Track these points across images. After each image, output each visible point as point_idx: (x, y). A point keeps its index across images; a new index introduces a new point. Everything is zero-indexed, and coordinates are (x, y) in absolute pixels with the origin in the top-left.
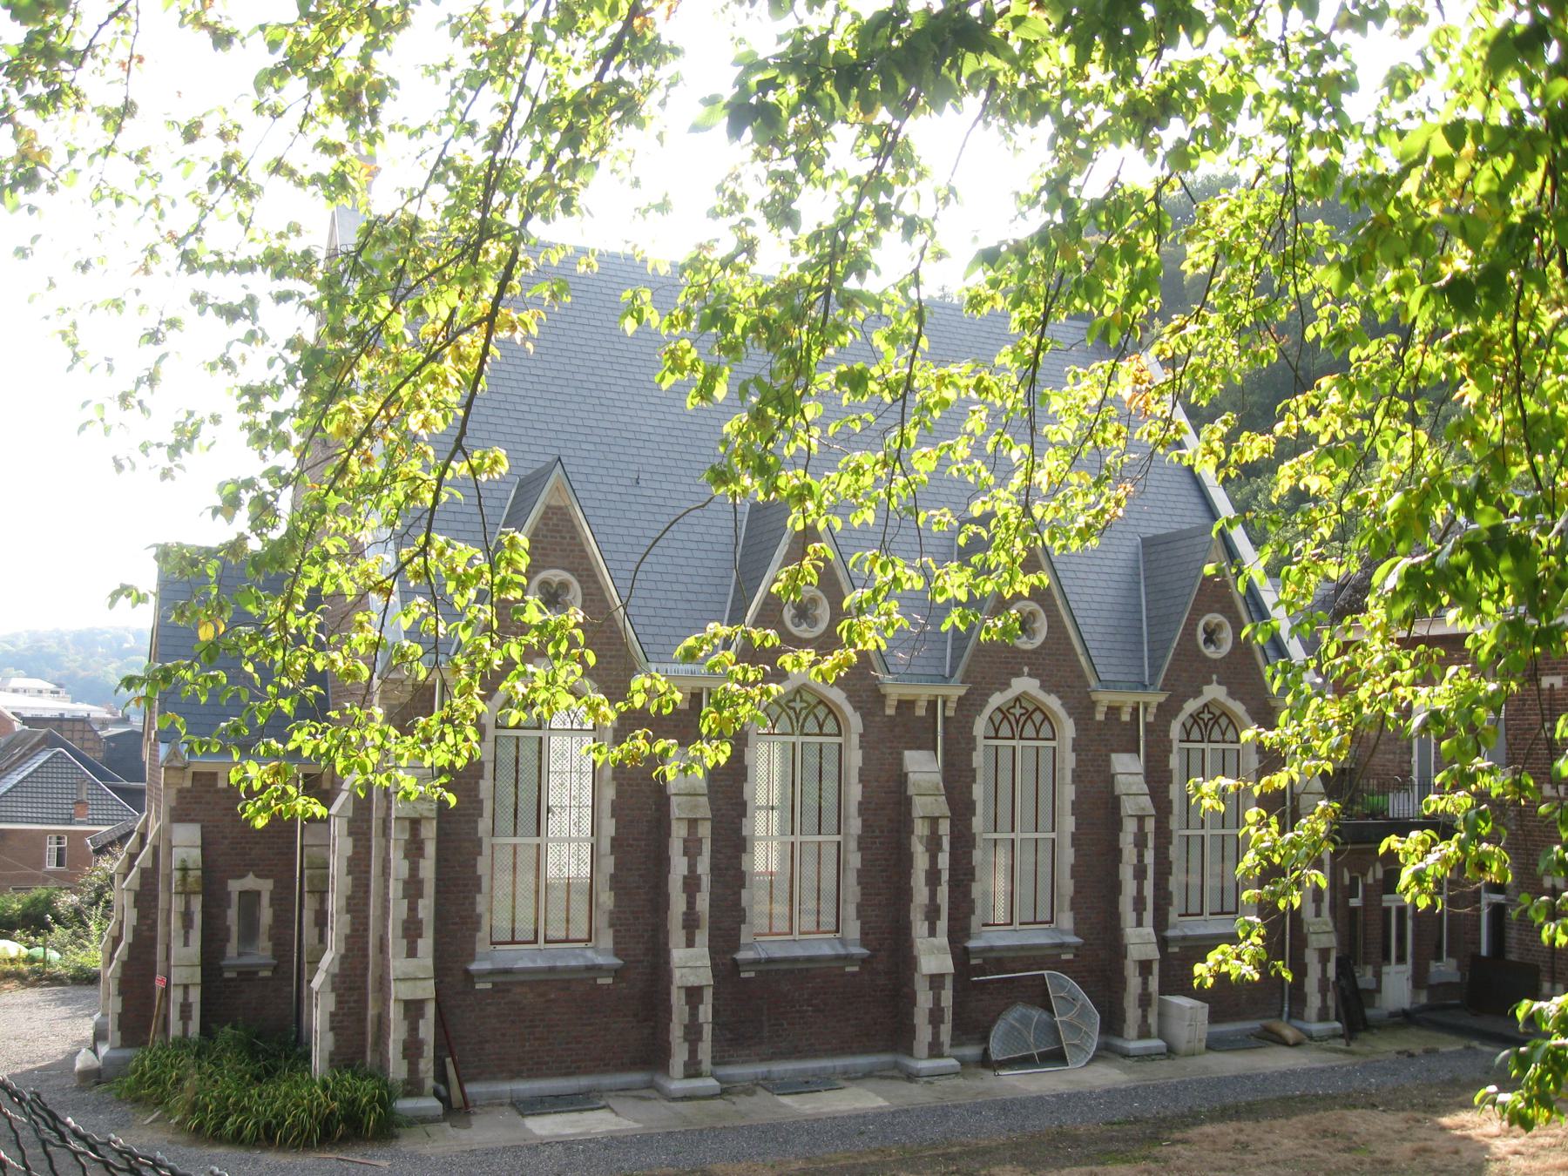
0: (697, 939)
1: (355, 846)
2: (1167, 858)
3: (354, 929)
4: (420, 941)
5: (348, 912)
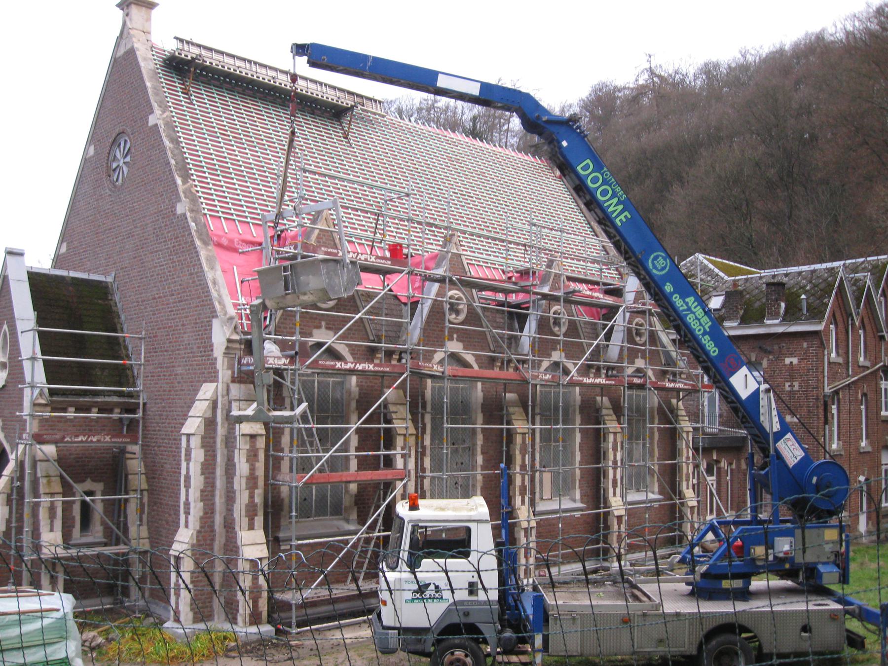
0: (256, 524)
1: (206, 455)
2: (281, 395)
3: (206, 513)
4: (256, 518)
5: (201, 501)
